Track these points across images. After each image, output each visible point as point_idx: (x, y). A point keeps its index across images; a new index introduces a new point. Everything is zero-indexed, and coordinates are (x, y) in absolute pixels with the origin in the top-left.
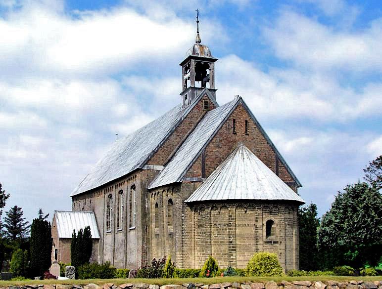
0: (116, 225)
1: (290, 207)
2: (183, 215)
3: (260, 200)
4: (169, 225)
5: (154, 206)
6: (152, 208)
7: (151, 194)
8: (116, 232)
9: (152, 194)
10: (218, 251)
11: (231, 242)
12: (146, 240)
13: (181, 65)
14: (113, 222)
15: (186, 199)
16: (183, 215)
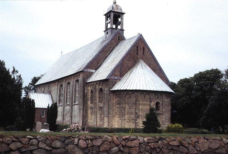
0: (65, 102)
1: (168, 96)
2: (109, 97)
3: (150, 90)
4: (99, 102)
5: (90, 92)
6: (88, 93)
7: (88, 85)
8: (65, 105)
9: (89, 85)
10: (129, 118)
11: (137, 113)
12: (85, 110)
13: (104, 15)
14: (63, 100)
15: (111, 88)
16: (109, 97)
